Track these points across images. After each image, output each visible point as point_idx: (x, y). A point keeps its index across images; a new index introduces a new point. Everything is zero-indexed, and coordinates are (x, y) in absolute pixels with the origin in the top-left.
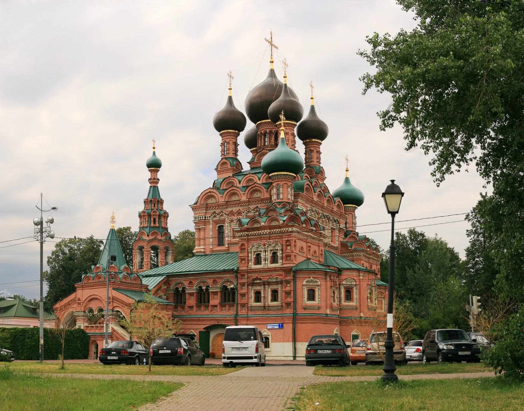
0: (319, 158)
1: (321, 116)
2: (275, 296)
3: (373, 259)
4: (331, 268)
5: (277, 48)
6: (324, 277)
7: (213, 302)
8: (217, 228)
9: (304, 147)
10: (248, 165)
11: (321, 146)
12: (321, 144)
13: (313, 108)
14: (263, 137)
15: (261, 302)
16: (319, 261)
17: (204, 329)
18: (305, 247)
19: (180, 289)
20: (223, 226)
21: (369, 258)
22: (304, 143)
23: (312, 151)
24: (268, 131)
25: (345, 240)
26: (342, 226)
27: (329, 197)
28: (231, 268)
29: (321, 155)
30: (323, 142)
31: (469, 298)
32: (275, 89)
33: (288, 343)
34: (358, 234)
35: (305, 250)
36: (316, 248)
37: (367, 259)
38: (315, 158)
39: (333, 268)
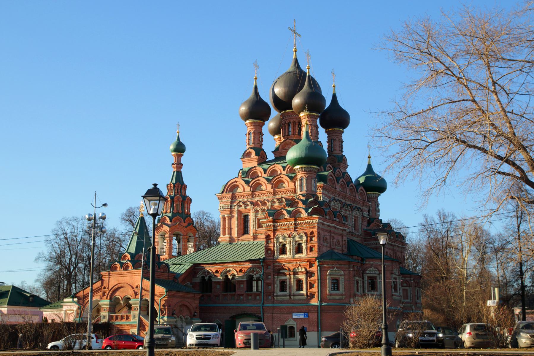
0: (341, 147)
1: (343, 103)
2: (300, 285)
3: (398, 247)
4: (354, 257)
5: (300, 35)
6: (347, 266)
7: (238, 292)
8: (242, 217)
9: (327, 135)
10: (273, 155)
11: (343, 135)
12: (343, 132)
13: (334, 97)
14: (287, 127)
15: (286, 291)
16: (343, 251)
17: (230, 318)
18: (328, 237)
19: (207, 278)
20: (248, 215)
21: (393, 246)
22: (326, 132)
23: (334, 140)
24: (292, 121)
25: (369, 228)
26: (366, 214)
27: (352, 186)
28: (258, 258)
29: (343, 144)
30: (345, 130)
31: (491, 290)
32: (321, 223)
33: (313, 332)
34: (381, 220)
35: (329, 240)
36: (340, 238)
37: (391, 247)
38: (338, 147)
39: (356, 258)
